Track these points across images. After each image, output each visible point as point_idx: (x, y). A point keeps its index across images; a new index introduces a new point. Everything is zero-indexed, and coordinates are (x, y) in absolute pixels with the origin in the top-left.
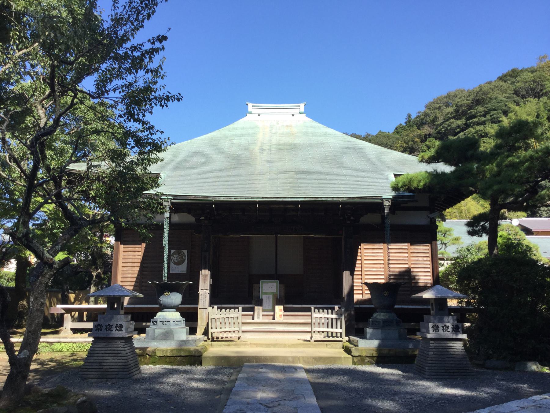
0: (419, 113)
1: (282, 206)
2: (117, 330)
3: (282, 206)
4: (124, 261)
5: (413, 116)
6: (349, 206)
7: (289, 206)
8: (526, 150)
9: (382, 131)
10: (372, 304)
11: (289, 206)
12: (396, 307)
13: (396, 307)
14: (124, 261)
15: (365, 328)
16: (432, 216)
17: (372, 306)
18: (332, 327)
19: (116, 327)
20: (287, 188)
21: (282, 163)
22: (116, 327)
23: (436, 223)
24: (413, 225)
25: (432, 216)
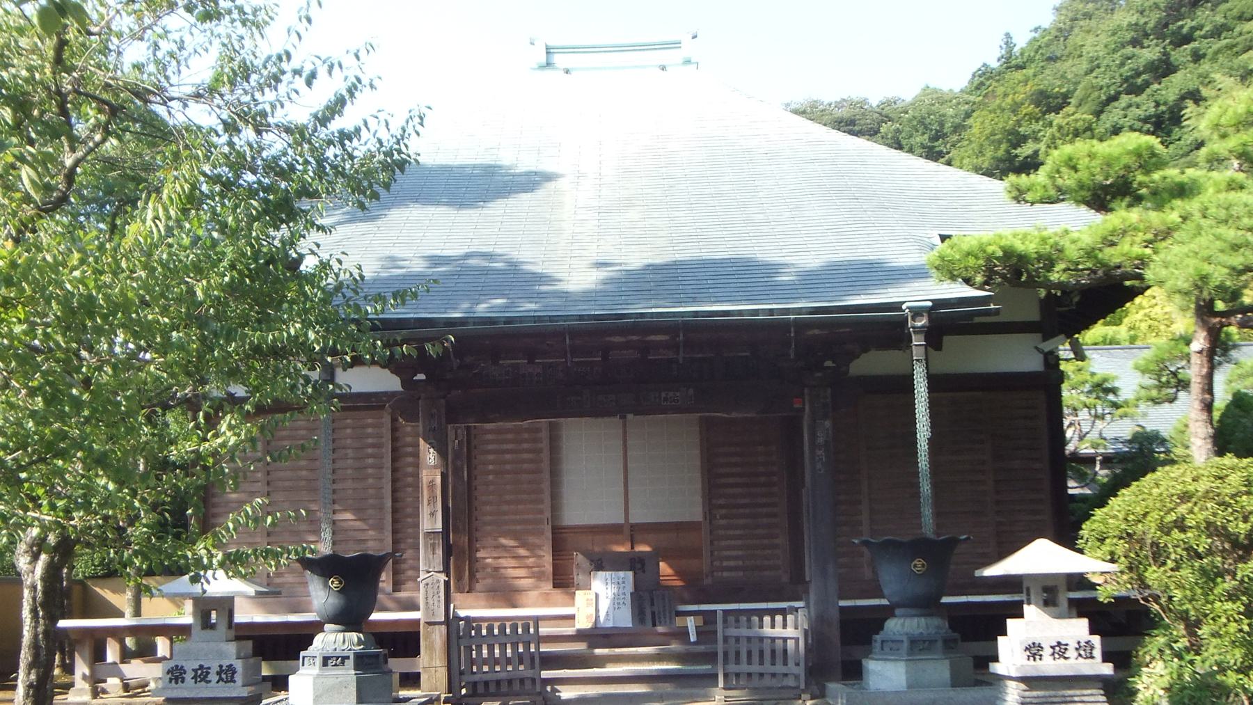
0: (1036, 30)
1: (635, 338)
2: (221, 679)
3: (635, 338)
4: (756, 658)
5: (1021, 41)
6: (816, 332)
7: (652, 338)
8: (226, 605)
9: (931, 86)
10: (883, 597)
11: (652, 338)
12: (945, 600)
13: (945, 600)
14: (756, 658)
15: (864, 662)
16: (1047, 346)
17: (885, 602)
18: (761, 663)
19: (218, 673)
20: (648, 286)
21: (633, 215)
22: (218, 673)
23: (1058, 365)
24: (988, 374)
25: (1047, 346)
